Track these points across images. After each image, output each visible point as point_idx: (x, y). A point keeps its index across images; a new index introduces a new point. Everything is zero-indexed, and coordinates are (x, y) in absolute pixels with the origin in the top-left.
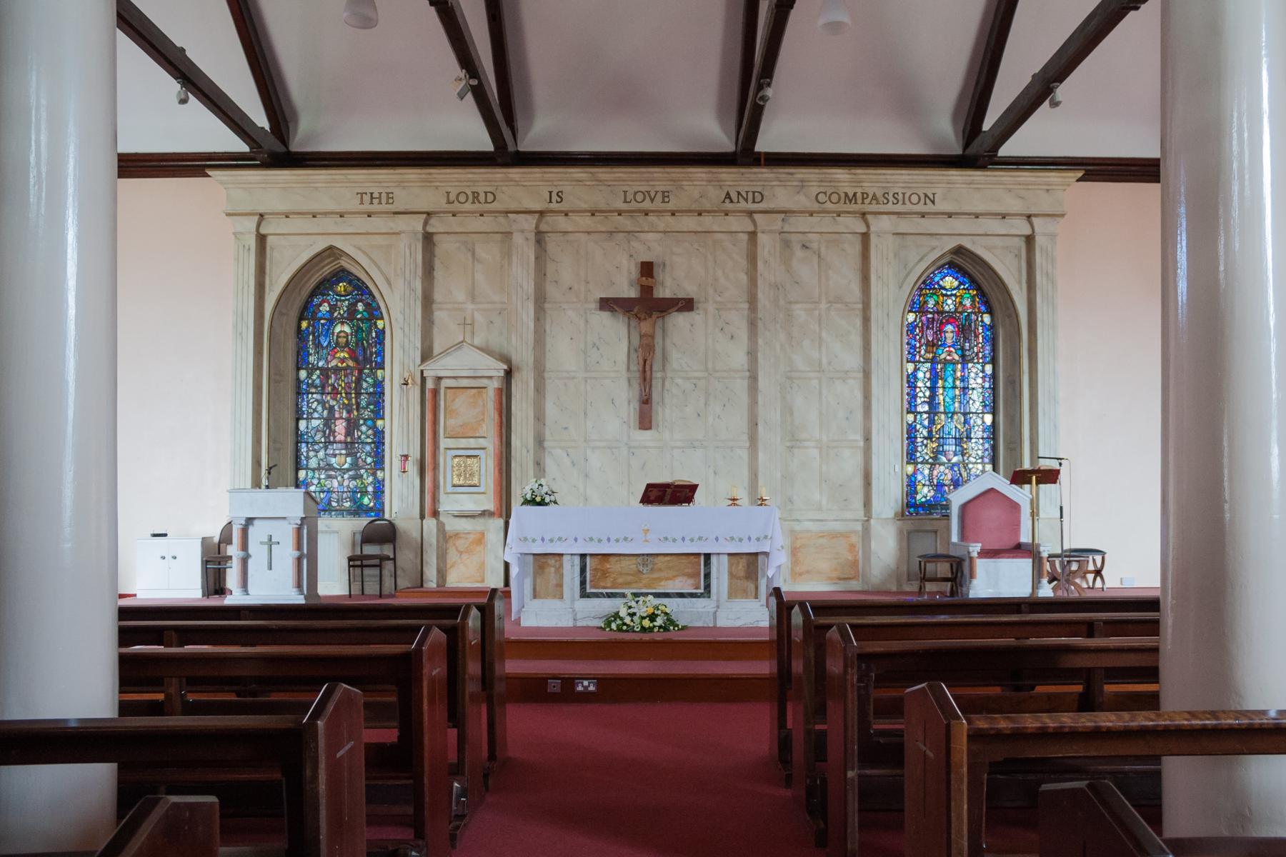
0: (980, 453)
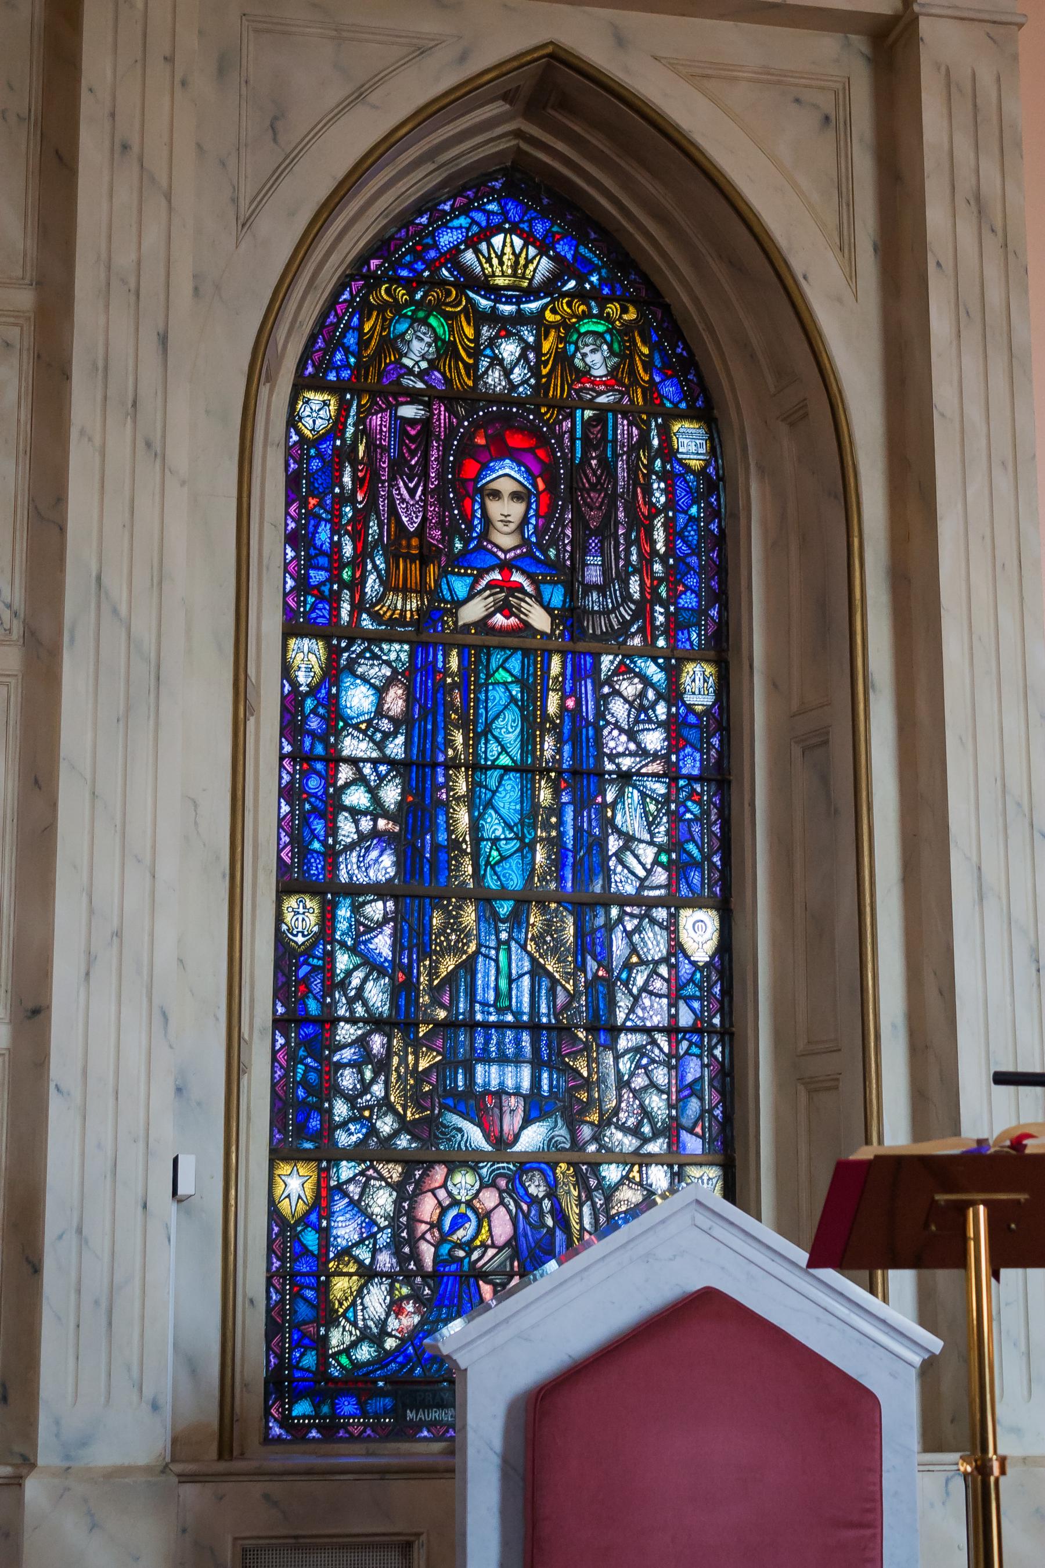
0: (656, 1103)
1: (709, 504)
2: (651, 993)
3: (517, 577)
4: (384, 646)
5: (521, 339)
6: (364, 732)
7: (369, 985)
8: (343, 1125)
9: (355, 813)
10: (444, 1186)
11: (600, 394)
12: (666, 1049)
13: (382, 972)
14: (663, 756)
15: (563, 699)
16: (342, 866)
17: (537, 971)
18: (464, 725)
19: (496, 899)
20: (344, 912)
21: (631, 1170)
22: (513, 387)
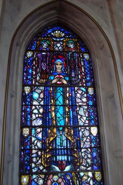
0: (89, 161)
1: (90, 65)
2: (87, 142)
3: (61, 76)
4: (40, 87)
5: (60, 44)
6: (37, 101)
7: (38, 143)
8: (34, 168)
9: (35, 114)
10: (52, 178)
11: (72, 50)
12: (90, 151)
13: (40, 141)
14: (86, 102)
15: (69, 94)
16: (33, 123)
17: (67, 139)
18: (53, 99)
19: (59, 127)
20: (33, 131)
21: (85, 173)
22: (59, 50)
